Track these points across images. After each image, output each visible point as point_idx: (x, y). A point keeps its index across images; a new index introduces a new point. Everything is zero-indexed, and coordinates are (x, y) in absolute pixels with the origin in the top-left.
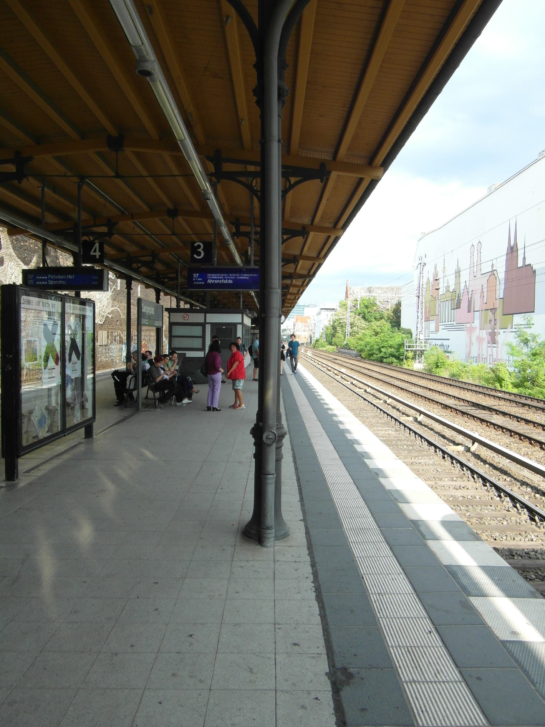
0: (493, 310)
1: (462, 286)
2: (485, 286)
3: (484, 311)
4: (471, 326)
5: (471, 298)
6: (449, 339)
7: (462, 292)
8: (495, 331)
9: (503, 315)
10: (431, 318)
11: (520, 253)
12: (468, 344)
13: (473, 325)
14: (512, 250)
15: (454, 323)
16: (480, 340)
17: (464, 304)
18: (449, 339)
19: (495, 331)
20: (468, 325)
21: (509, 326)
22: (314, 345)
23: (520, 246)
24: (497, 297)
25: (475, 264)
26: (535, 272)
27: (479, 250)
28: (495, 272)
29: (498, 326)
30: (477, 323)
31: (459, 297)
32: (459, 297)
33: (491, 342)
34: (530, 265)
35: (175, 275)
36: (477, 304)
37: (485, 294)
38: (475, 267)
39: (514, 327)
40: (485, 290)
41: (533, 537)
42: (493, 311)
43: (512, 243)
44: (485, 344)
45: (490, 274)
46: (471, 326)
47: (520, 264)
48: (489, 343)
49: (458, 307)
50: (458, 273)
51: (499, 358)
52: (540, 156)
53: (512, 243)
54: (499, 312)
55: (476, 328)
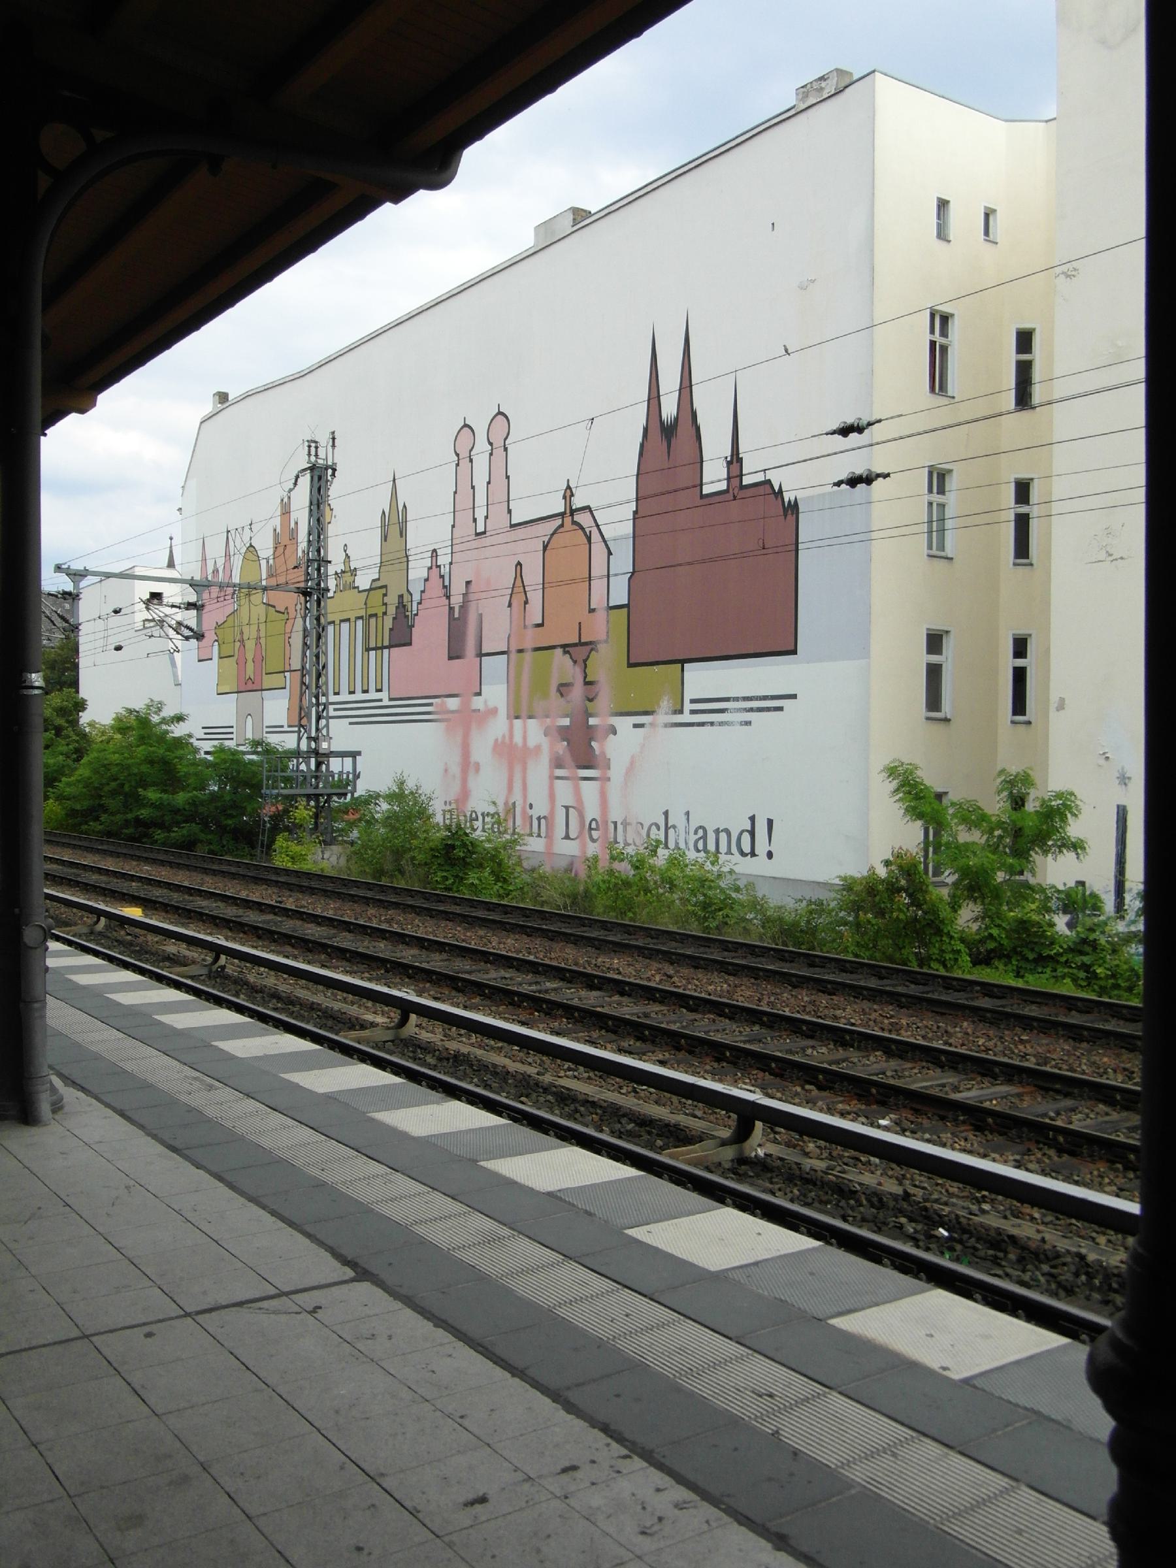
0: (579, 649)
1: (418, 570)
3: (528, 656)
4: (466, 704)
5: (464, 607)
8: (592, 721)
9: (630, 665)
10: (268, 681)
11: (715, 447)
12: (456, 770)
13: (478, 703)
14: (669, 438)
15: (384, 695)
16: (512, 755)
17: (430, 630)
19: (592, 721)
20: (453, 704)
21: (665, 704)
22: (741, 1151)
24: (598, 600)
27: (498, 443)
28: (584, 519)
29: (604, 700)
30: (495, 694)
33: (568, 759)
35: (102, 919)
36: (496, 624)
39: (688, 706)
40: (533, 576)
42: (581, 652)
43: (669, 409)
44: (539, 772)
46: (466, 704)
47: (714, 477)
48: (559, 766)
49: (401, 636)
50: (394, 525)
51: (615, 814)
52: (806, 96)
53: (669, 409)
54: (607, 662)
55: (494, 711)
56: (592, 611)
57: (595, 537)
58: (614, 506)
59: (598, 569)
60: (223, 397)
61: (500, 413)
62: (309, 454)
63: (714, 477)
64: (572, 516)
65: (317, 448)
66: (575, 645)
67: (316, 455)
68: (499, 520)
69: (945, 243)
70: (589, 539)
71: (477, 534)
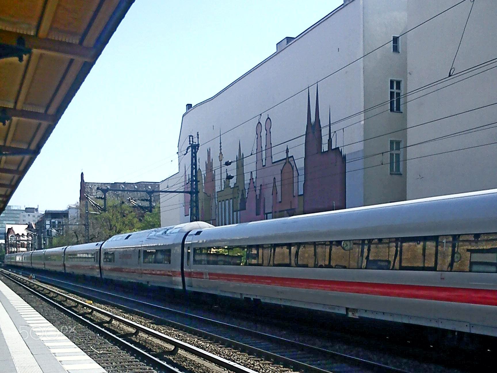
2: (278, 178)
5: (260, 195)
6: (82, 174)
7: (247, 187)
11: (325, 132)
14: (313, 129)
18: (82, 174)
23: (324, 122)
25: (264, 148)
26: (345, 157)
31: (243, 195)
32: (243, 195)
34: (292, 156)
37: (279, 189)
38: (264, 152)
40: (278, 184)
41: (130, 217)
45: (285, 161)
47: (325, 148)
53: (313, 119)
56: (294, 196)
57: (294, 168)
58: (299, 153)
59: (295, 180)
60: (189, 106)
61: (268, 118)
62: (190, 141)
63: (325, 148)
64: (288, 160)
65: (190, 141)
66: (290, 210)
67: (192, 141)
68: (269, 164)
69: (397, 53)
70: (293, 169)
71: (263, 166)
